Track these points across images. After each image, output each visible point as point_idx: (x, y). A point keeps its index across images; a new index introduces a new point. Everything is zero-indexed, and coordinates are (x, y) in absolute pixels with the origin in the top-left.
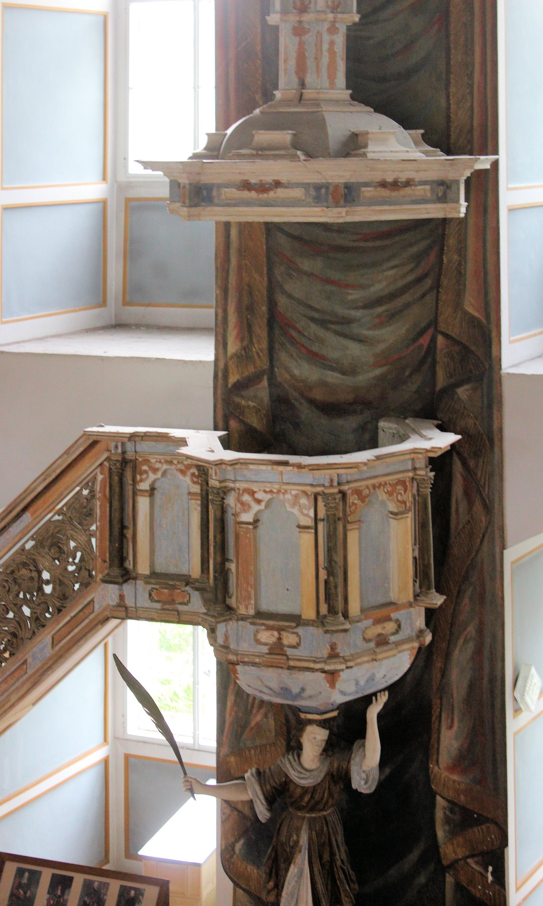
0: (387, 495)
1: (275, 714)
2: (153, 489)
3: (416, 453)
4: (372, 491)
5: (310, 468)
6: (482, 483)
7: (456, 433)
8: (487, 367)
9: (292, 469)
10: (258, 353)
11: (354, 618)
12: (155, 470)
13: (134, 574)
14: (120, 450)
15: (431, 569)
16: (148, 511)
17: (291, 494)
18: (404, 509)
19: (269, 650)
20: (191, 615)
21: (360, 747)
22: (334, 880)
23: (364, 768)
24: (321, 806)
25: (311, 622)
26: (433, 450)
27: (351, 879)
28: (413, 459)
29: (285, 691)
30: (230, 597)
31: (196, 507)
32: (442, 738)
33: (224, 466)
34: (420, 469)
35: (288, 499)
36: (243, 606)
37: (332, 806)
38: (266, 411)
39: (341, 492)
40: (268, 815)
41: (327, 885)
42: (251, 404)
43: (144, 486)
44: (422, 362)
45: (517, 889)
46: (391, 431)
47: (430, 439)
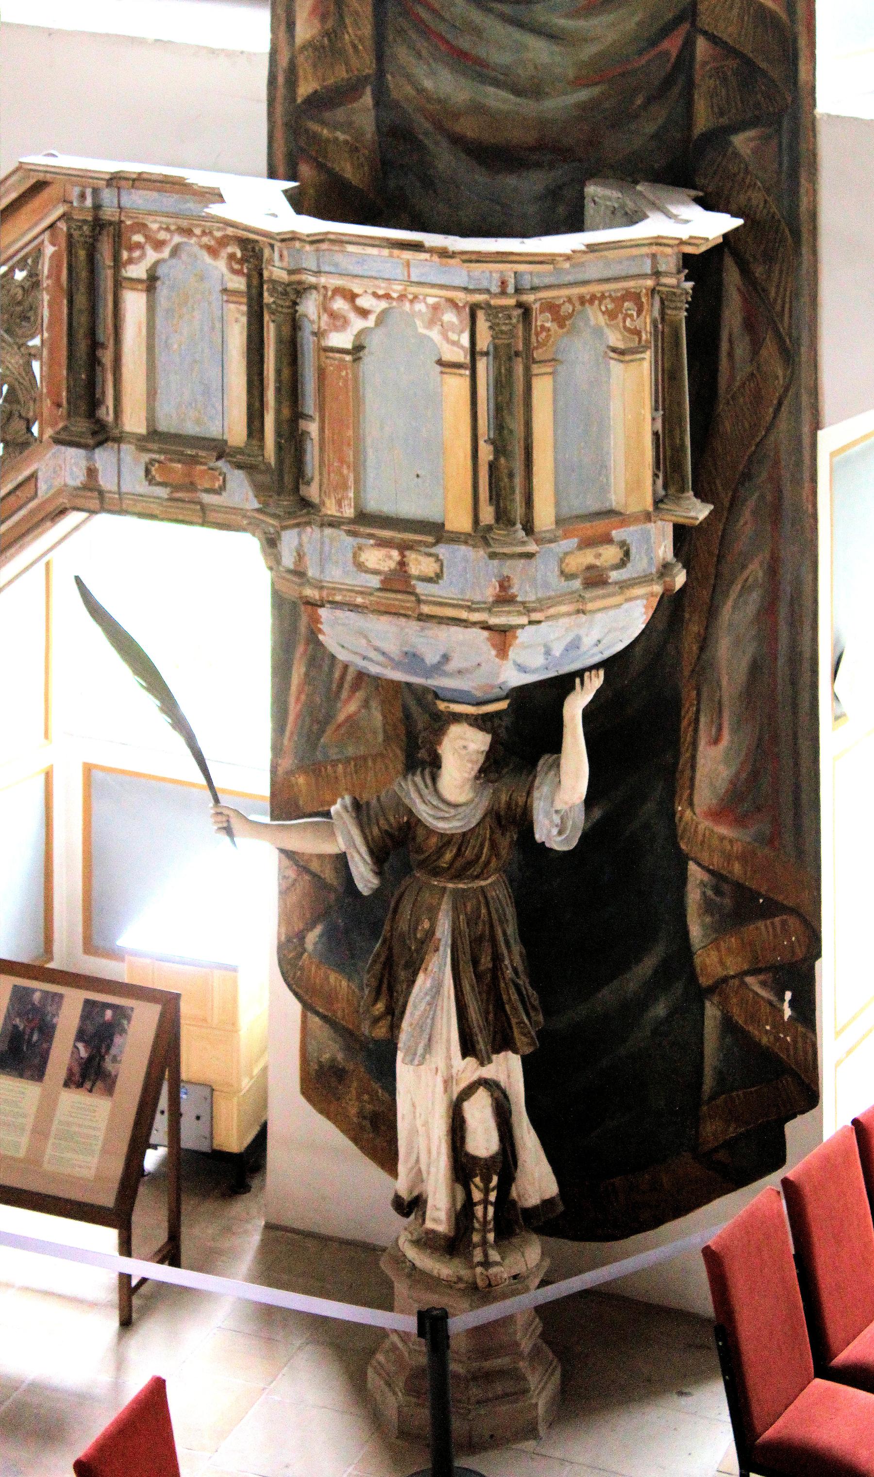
0: (606, 317)
1: (383, 702)
2: (151, 282)
3: (660, 244)
4: (578, 307)
5: (465, 257)
6: (778, 308)
7: (735, 215)
8: (789, 99)
9: (428, 258)
10: (355, 47)
11: (544, 535)
12: (159, 245)
13: (116, 432)
14: (89, 202)
15: (686, 454)
16: (144, 319)
17: (426, 303)
18: (636, 344)
19: (382, 582)
20: (226, 513)
21: (550, 768)
22: (499, 1006)
23: (558, 805)
24: (477, 870)
25: (463, 537)
26: (692, 241)
27: (530, 1003)
28: (654, 256)
29: (412, 660)
30: (308, 483)
31: (239, 316)
32: (701, 761)
33: (297, 244)
34: (667, 274)
35: (420, 311)
36: (333, 501)
37: (497, 870)
38: (369, 152)
39: (519, 305)
40: (375, 882)
41: (487, 1013)
42: (341, 136)
43: (137, 271)
44: (668, 82)
45: (838, 1033)
46: (608, 203)
47: (687, 221)
